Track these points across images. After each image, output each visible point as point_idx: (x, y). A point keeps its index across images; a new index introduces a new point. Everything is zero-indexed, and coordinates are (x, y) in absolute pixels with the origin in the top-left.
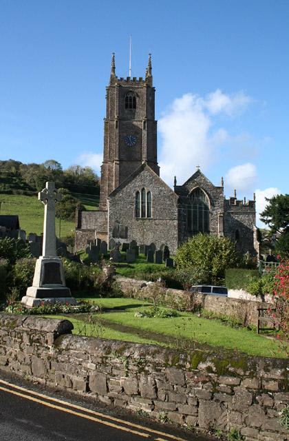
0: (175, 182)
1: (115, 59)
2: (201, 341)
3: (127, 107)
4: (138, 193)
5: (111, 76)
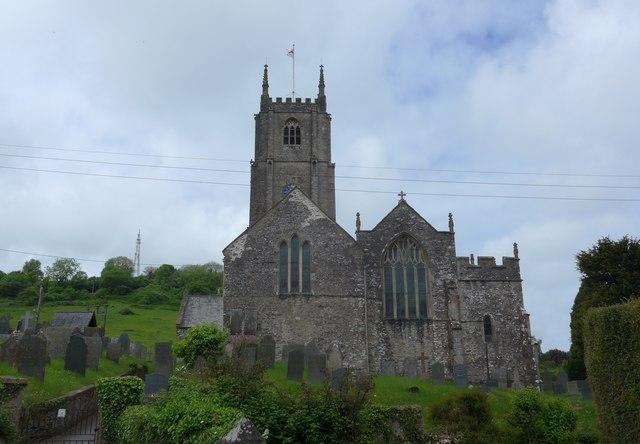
0: (358, 223)
1: (268, 74)
3: (286, 142)
4: (283, 243)
5: (262, 97)
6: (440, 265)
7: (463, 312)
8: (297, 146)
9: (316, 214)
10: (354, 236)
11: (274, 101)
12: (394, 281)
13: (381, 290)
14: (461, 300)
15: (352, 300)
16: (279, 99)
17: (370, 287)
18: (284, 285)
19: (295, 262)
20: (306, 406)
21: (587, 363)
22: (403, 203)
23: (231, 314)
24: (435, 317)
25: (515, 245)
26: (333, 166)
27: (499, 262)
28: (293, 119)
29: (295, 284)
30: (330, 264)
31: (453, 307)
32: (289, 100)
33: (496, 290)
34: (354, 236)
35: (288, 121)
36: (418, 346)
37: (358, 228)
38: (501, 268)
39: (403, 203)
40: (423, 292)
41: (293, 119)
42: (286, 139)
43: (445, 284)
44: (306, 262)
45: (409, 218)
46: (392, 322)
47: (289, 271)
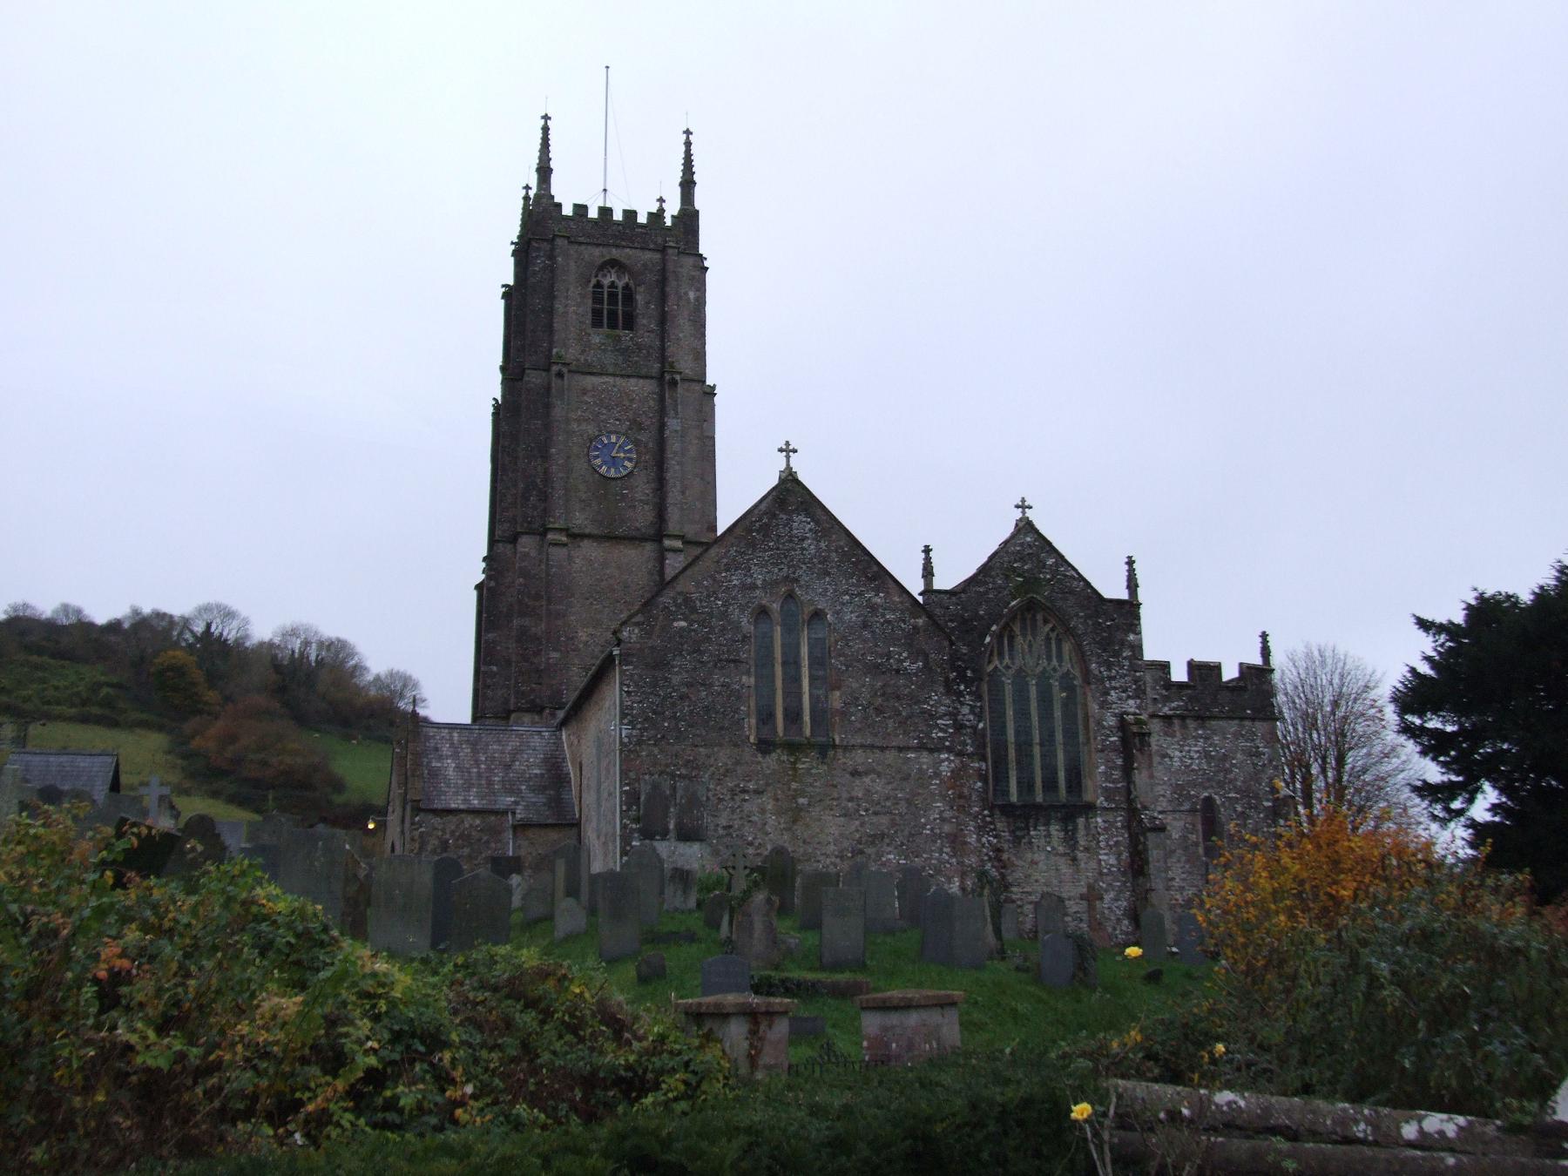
0: (928, 572)
3: (597, 322)
6: (1111, 678)
8: (626, 336)
11: (567, 211)
12: (1010, 713)
13: (984, 736)
15: (925, 758)
18: (766, 717)
19: (792, 663)
21: (511, 832)
22: (1025, 527)
23: (644, 789)
24: (1101, 801)
25: (1264, 636)
26: (711, 393)
27: (1230, 673)
28: (613, 263)
39: (1025, 527)
43: (1123, 725)
44: (817, 662)
46: (1008, 810)
47: (779, 683)
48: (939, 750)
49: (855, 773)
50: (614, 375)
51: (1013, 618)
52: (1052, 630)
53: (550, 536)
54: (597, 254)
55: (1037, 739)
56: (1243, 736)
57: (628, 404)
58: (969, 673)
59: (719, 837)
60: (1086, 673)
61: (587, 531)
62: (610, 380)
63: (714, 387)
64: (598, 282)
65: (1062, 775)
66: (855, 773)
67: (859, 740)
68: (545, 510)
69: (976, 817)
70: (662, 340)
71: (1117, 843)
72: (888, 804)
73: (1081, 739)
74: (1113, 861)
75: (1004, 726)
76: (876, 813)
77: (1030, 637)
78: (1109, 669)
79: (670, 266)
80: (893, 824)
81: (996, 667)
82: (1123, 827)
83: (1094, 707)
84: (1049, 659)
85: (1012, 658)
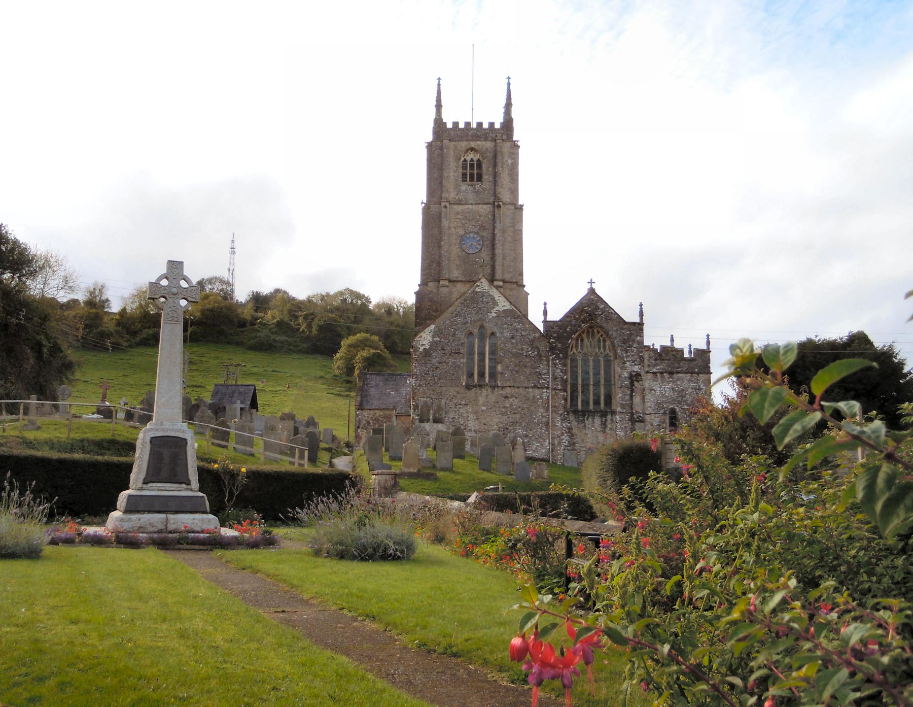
0: (545, 313)
2: (841, 339)
3: (464, 179)
6: (628, 356)
7: (648, 404)
8: (478, 186)
9: (503, 304)
10: (541, 327)
11: (449, 125)
13: (566, 381)
14: (647, 392)
15: (537, 391)
16: (456, 124)
17: (555, 378)
18: (470, 375)
19: (482, 355)
20: (733, 482)
22: (592, 291)
26: (521, 208)
28: (472, 149)
29: (481, 375)
30: (516, 355)
31: (637, 400)
32: (468, 124)
33: (685, 382)
34: (541, 327)
35: (467, 151)
36: (601, 437)
37: (545, 318)
38: (690, 360)
39: (592, 291)
40: (608, 381)
41: (472, 149)
42: (464, 175)
44: (493, 352)
45: (597, 308)
46: (576, 412)
47: (476, 361)
48: (542, 388)
49: (506, 397)
50: (472, 204)
51: (583, 332)
52: (602, 336)
53: (442, 283)
54: (464, 145)
55: (592, 383)
56: (692, 381)
57: (478, 217)
58: (561, 355)
59: (449, 422)
60: (615, 354)
61: (459, 279)
62: (470, 206)
63: (522, 206)
64: (465, 159)
65: (602, 398)
66: (506, 397)
67: (508, 384)
68: (440, 270)
69: (561, 415)
70: (495, 185)
71: (626, 427)
72: (520, 409)
73: (612, 382)
74: (622, 434)
75: (577, 377)
76: (514, 413)
77: (591, 340)
78: (627, 352)
79: (498, 149)
80: (521, 417)
81: (574, 353)
82: (629, 420)
83: (618, 369)
84: (599, 348)
85: (582, 348)
